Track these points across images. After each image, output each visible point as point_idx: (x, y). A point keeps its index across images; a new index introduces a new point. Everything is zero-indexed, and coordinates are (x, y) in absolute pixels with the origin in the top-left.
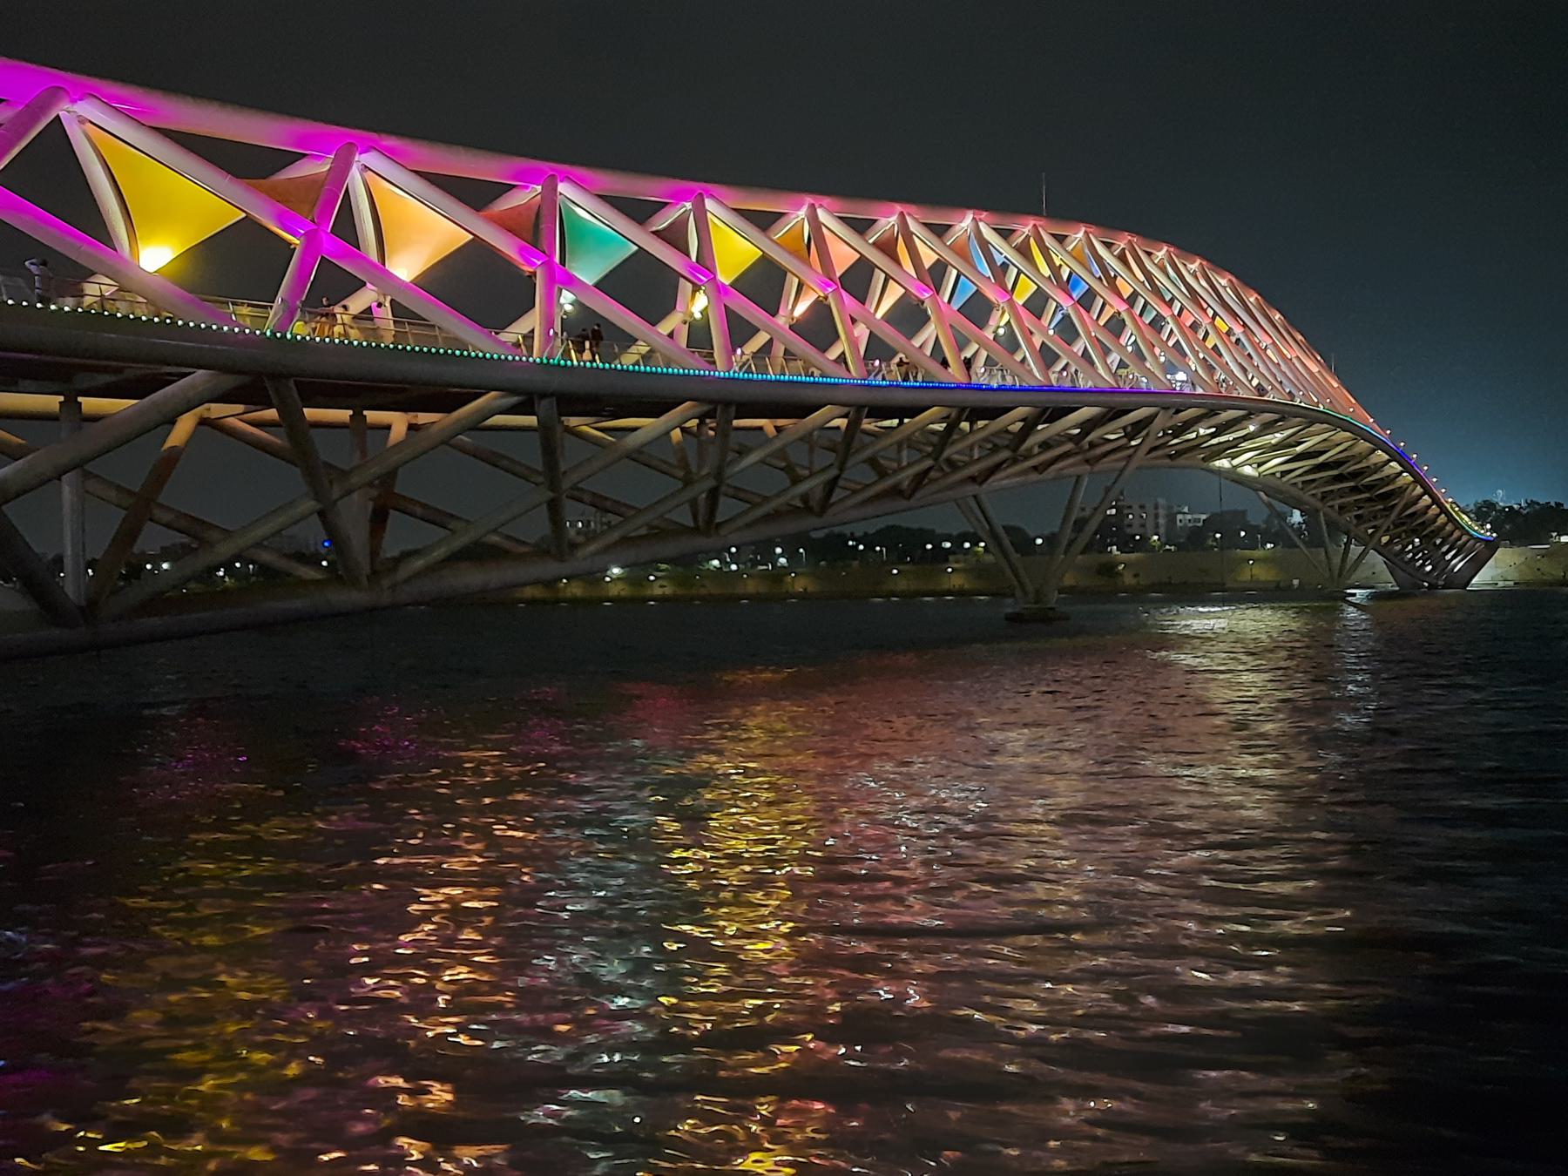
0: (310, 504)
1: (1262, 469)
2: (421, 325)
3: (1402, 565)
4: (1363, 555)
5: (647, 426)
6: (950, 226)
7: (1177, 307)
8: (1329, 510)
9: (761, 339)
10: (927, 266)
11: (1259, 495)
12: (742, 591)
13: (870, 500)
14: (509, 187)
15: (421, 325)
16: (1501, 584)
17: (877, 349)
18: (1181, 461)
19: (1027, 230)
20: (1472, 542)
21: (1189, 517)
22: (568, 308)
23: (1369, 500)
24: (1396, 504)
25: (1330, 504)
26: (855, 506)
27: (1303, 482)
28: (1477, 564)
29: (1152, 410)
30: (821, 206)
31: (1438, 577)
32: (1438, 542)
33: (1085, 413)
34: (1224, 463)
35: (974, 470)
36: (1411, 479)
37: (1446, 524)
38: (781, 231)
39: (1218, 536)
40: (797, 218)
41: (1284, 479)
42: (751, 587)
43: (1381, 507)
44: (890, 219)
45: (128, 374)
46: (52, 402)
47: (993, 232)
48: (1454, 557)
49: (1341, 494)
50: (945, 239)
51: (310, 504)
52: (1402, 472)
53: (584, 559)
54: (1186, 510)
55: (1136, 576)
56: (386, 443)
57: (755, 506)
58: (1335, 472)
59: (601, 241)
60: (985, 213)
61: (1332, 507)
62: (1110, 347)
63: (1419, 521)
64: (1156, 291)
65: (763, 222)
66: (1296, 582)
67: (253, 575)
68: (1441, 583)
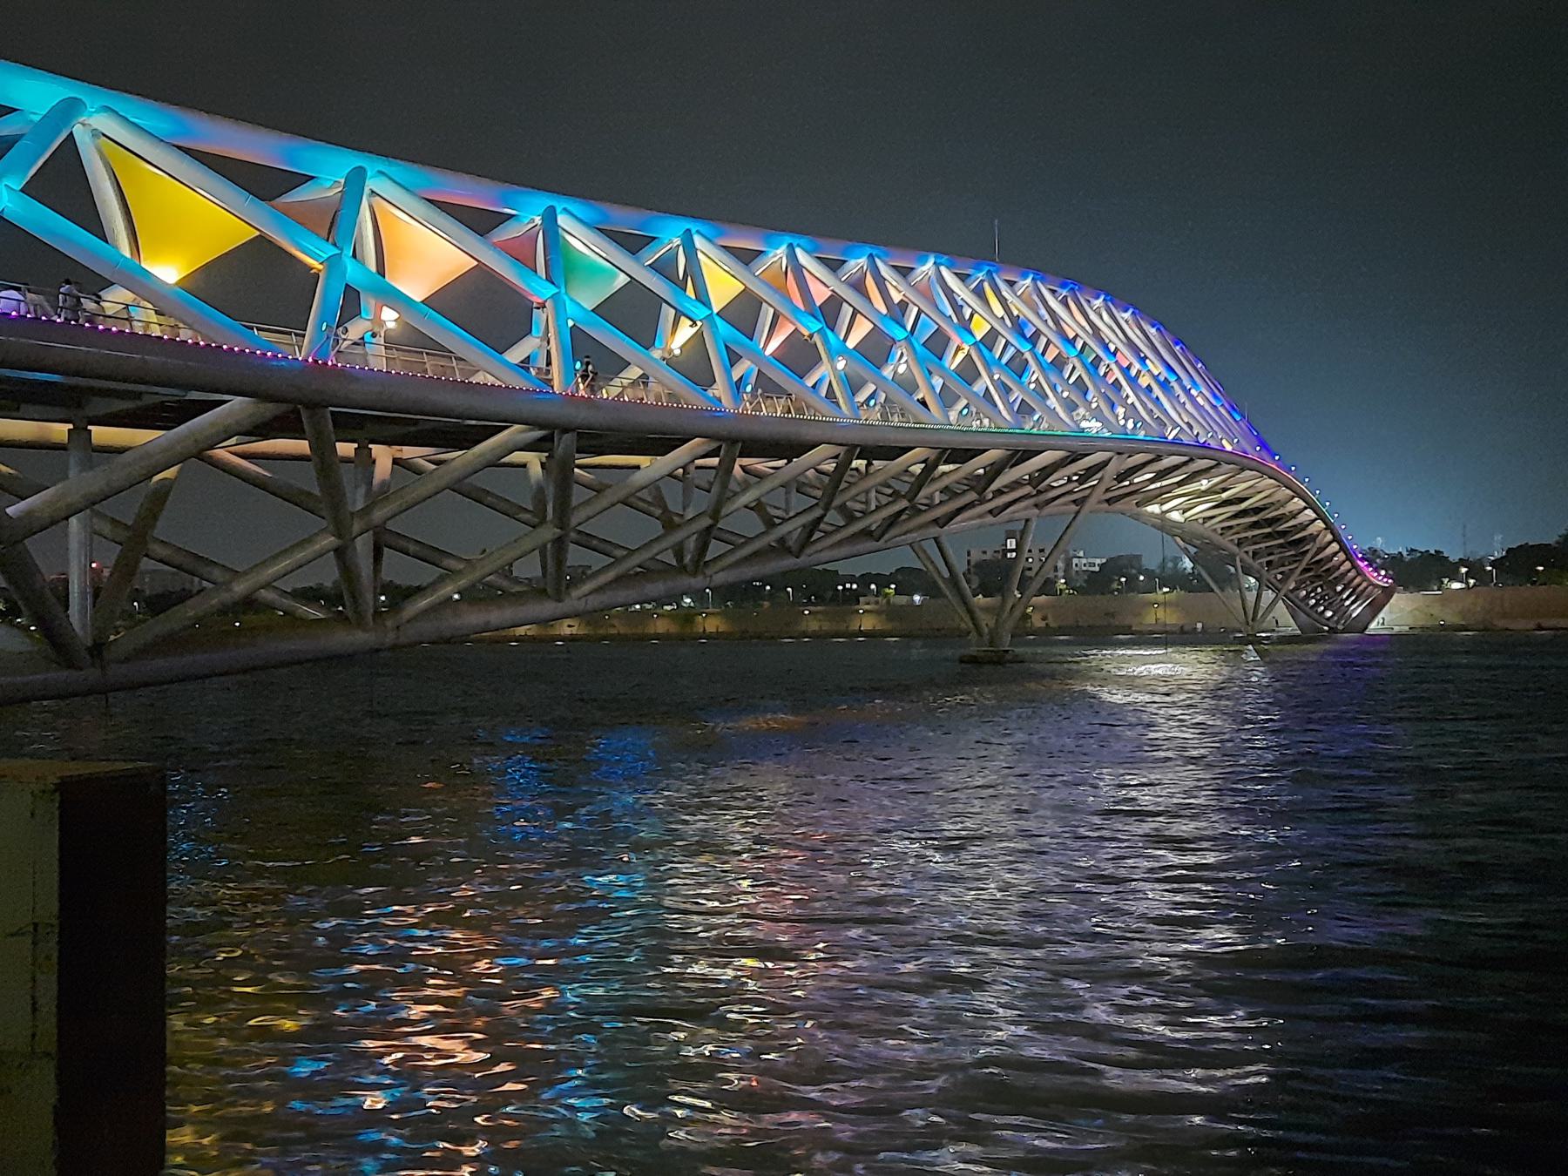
0: (329, 541)
1: (1188, 514)
2: (443, 356)
3: (1315, 615)
4: (1274, 602)
5: (650, 466)
6: (845, 261)
7: (1079, 345)
8: (1245, 556)
9: (634, 372)
10: (818, 304)
11: (1175, 541)
12: (652, 632)
13: (840, 543)
14: (504, 217)
15: (443, 356)
16: (1397, 629)
17: (766, 386)
18: (1118, 506)
19: (981, 276)
20: (1371, 588)
21: (1084, 561)
22: (391, 325)
23: (1281, 546)
24: (1307, 551)
25: (1246, 549)
26: (832, 547)
27: (1222, 529)
28: (1375, 608)
29: (1108, 455)
30: (799, 246)
31: (1337, 622)
32: (1339, 588)
33: (993, 455)
34: (1154, 509)
35: (939, 512)
36: (1324, 526)
37: (1349, 571)
38: (760, 267)
39: (1123, 580)
40: (777, 254)
41: (1207, 525)
42: (661, 626)
43: (1293, 553)
44: (778, 252)
45: (148, 400)
46: (59, 431)
47: (954, 276)
48: (1353, 603)
49: (1255, 540)
50: (910, 279)
51: (329, 541)
52: (1316, 519)
53: (580, 598)
54: (1081, 554)
55: (1044, 619)
56: (529, 481)
57: (737, 547)
58: (1254, 519)
59: (594, 270)
60: (946, 257)
61: (1247, 552)
62: (1012, 386)
63: (1324, 568)
64: (1062, 334)
65: (746, 258)
66: (1199, 626)
67: (139, 613)
68: (1340, 627)
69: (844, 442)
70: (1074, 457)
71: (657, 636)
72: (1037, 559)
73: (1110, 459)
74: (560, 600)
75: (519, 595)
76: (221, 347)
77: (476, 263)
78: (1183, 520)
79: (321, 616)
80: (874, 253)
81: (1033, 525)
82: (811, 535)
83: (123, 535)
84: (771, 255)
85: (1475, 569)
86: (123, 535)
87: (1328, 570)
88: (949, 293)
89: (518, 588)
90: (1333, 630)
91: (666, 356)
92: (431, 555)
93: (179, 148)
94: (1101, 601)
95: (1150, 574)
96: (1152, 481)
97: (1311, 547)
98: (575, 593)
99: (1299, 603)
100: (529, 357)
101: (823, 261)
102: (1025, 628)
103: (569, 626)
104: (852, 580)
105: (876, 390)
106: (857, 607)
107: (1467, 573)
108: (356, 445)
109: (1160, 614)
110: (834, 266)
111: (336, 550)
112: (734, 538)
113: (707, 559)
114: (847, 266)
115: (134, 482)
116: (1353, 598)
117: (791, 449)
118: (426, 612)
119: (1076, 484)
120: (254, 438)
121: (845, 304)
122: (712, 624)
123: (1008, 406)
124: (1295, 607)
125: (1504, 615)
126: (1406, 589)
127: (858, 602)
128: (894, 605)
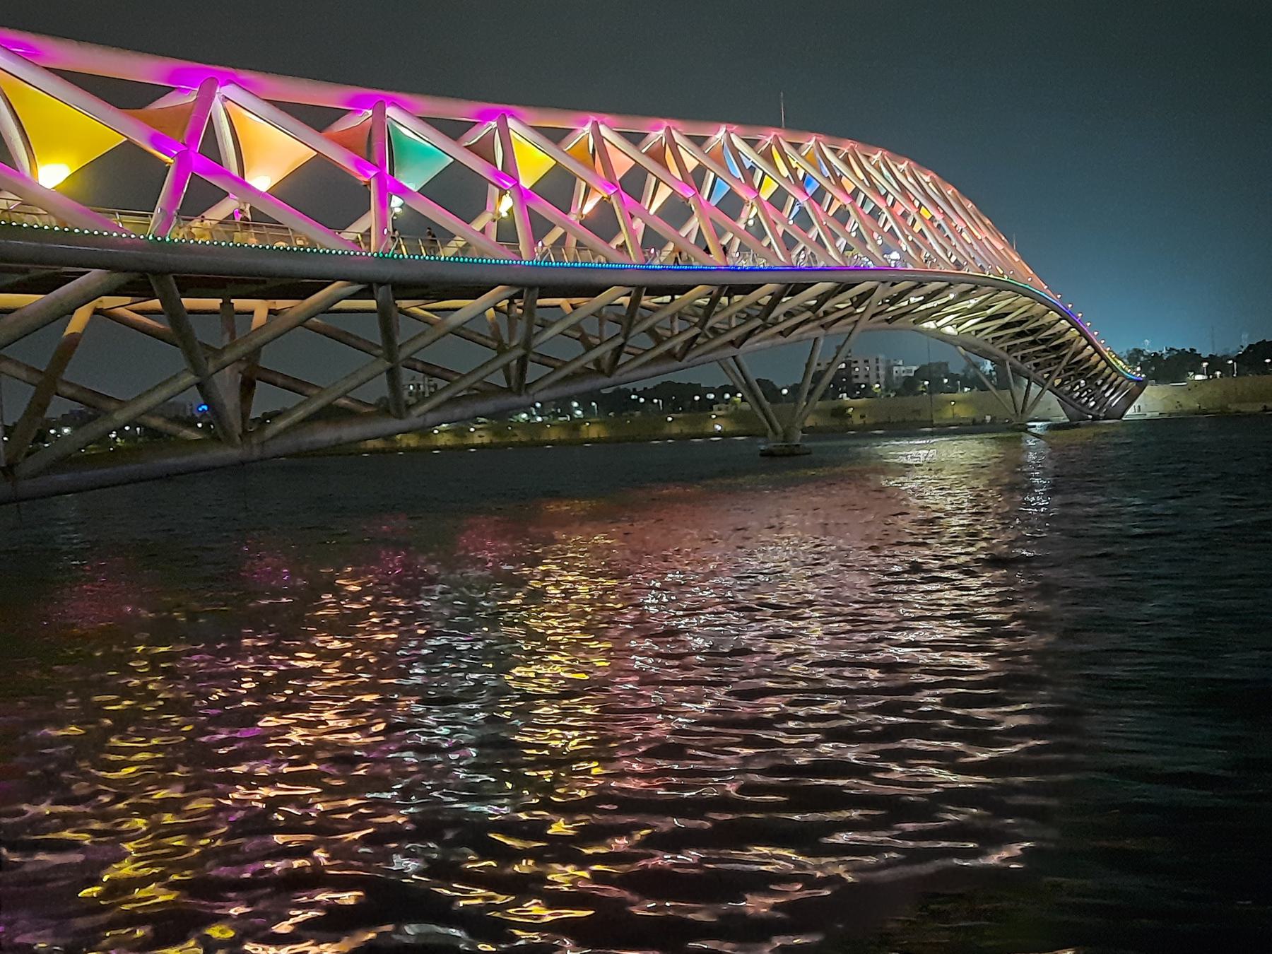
0: (190, 378)
3: (1079, 406)
5: (468, 307)
8: (1015, 361)
10: (690, 171)
18: (896, 324)
20: (1126, 382)
21: (903, 368)
23: (1045, 351)
24: (1065, 355)
25: (1015, 354)
27: (993, 338)
28: (1130, 399)
30: (602, 123)
33: (821, 287)
34: (931, 325)
36: (1078, 333)
37: (1105, 369)
38: (570, 143)
39: (927, 383)
41: (978, 336)
42: (554, 435)
43: (1054, 356)
46: (215, 303)
48: (1112, 394)
49: (1024, 346)
51: (190, 378)
52: (1070, 328)
54: (901, 363)
57: (556, 369)
59: (424, 153)
61: (1016, 357)
64: (874, 187)
65: (556, 136)
66: (988, 418)
68: (1102, 415)
69: (632, 284)
70: (920, 285)
71: (552, 443)
72: (862, 369)
73: (877, 287)
74: (401, 418)
75: (368, 415)
76: (43, 228)
77: (316, 153)
78: (956, 333)
79: (200, 437)
80: (778, 134)
81: (821, 342)
82: (618, 357)
83: (37, 379)
84: (580, 132)
85: (1216, 363)
86: (37, 379)
87: (1087, 368)
88: (828, 163)
89: (366, 410)
90: (1095, 418)
91: (496, 217)
92: (295, 386)
93: (47, 68)
94: (909, 400)
95: (953, 378)
96: (922, 303)
97: (1068, 352)
98: (415, 412)
99: (1064, 397)
100: (484, 228)
101: (623, 134)
102: (847, 425)
103: (480, 437)
104: (711, 390)
105: (565, 234)
106: (709, 413)
107: (1207, 367)
108: (220, 301)
109: (957, 410)
110: (635, 139)
111: (198, 385)
112: (553, 362)
113: (527, 382)
114: (649, 138)
115: (18, 337)
116: (1112, 390)
117: (592, 291)
118: (286, 431)
119: (888, 305)
120: (143, 299)
121: (649, 175)
122: (593, 431)
123: (836, 249)
124: (1065, 400)
125: (1240, 400)
126: (1157, 382)
127: (711, 409)
128: (741, 410)
